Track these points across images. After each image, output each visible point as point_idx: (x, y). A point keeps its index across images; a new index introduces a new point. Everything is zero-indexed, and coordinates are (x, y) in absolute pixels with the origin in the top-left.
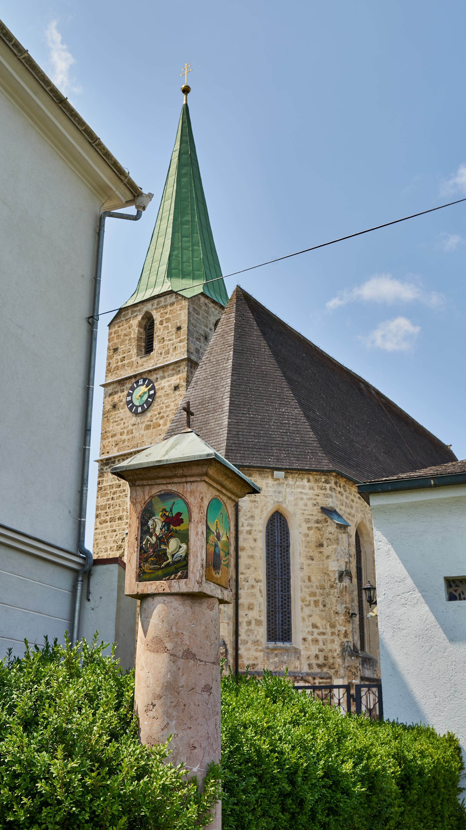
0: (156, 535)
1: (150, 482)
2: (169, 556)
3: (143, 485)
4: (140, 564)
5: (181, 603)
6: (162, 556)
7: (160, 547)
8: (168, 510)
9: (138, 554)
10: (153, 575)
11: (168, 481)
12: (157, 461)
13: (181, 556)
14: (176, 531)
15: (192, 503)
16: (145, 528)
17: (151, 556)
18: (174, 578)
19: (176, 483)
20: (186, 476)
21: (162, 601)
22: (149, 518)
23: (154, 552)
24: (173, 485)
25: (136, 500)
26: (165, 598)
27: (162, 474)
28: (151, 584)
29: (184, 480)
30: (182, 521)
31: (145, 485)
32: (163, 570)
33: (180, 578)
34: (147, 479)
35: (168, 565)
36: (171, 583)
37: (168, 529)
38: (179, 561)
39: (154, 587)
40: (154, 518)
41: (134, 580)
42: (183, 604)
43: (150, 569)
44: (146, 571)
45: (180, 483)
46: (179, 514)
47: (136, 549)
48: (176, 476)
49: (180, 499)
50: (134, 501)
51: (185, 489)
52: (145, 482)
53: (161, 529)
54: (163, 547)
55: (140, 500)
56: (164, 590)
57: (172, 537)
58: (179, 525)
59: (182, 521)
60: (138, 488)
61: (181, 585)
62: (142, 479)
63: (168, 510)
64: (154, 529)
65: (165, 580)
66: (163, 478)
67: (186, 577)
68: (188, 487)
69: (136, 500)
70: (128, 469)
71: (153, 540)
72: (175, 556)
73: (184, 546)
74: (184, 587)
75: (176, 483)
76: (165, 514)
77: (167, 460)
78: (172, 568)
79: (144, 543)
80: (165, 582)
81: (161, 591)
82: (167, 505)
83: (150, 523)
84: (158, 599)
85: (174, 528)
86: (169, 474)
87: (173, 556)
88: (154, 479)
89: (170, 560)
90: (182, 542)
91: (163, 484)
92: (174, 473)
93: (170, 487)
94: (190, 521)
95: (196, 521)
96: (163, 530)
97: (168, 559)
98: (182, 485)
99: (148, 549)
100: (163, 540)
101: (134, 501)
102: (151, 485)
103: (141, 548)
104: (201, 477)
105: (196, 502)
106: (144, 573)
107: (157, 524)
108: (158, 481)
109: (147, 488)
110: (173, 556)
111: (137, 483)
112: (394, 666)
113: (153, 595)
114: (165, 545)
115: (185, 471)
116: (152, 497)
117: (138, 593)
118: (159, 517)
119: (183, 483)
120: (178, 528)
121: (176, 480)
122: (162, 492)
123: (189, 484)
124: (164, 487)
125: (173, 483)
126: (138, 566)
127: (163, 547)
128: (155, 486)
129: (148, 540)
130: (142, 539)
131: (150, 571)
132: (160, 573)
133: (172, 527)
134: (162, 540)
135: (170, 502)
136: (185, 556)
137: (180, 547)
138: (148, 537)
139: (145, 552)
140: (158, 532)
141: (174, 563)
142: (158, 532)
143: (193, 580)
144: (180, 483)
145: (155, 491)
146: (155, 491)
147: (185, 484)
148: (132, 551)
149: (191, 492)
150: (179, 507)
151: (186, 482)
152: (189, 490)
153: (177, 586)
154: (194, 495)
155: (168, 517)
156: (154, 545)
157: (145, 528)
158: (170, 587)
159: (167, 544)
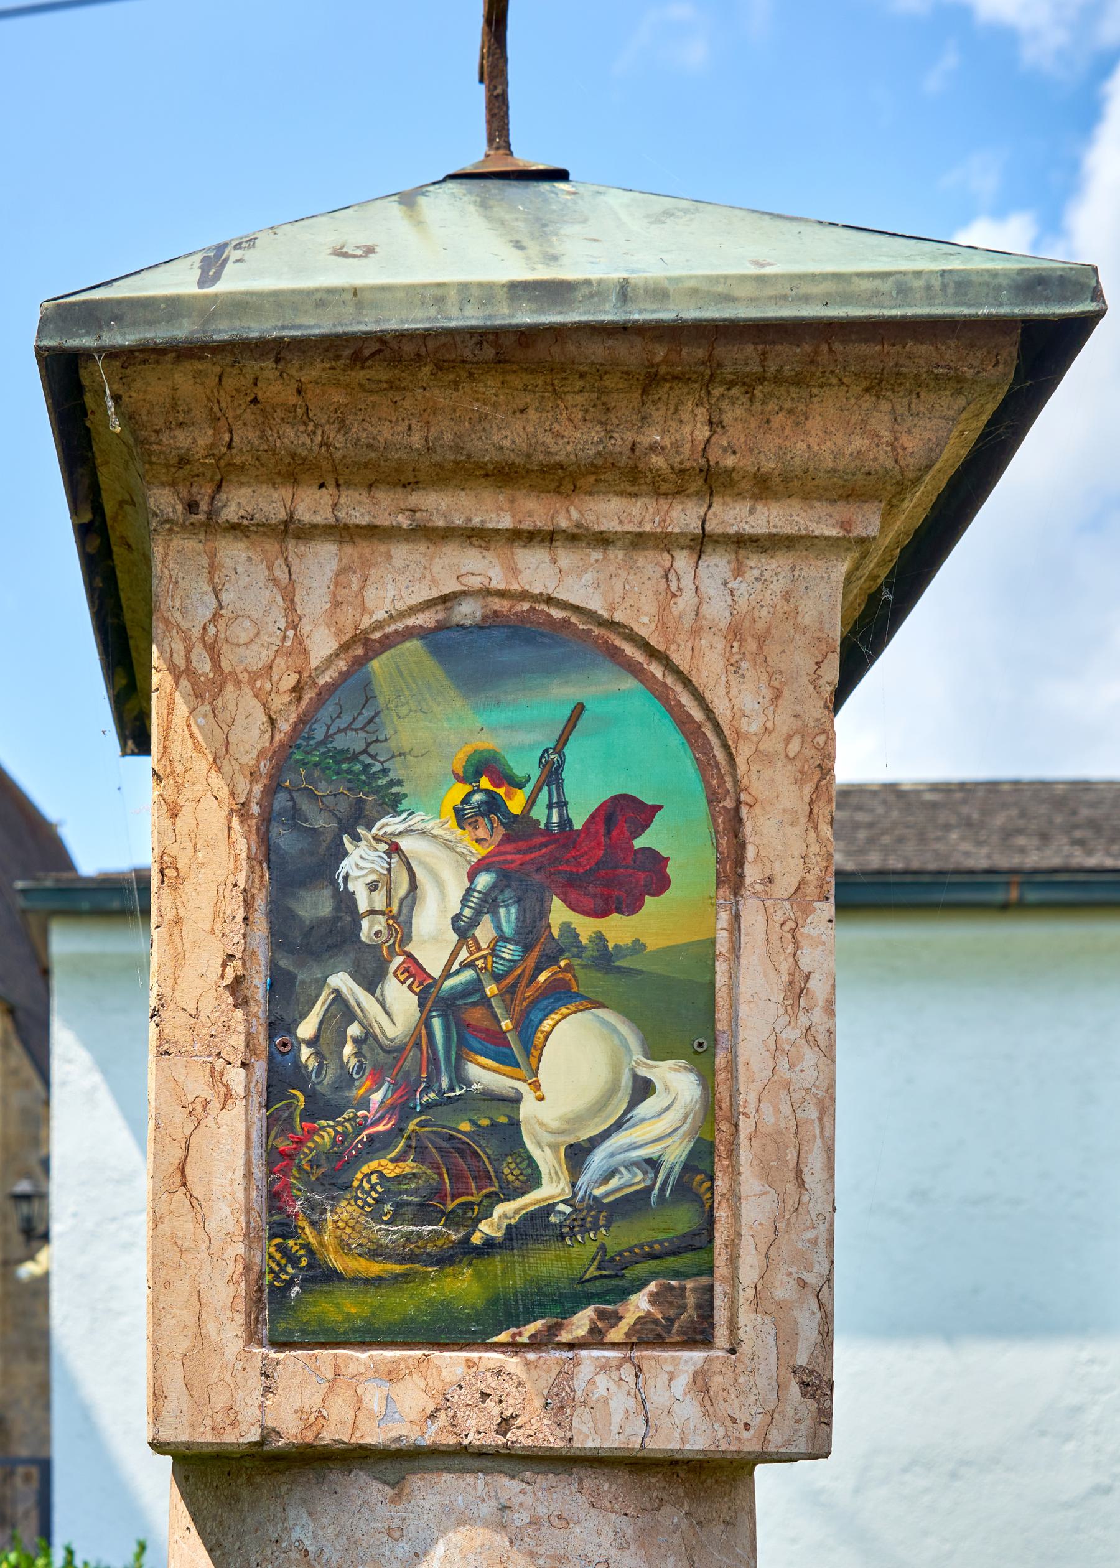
0: (413, 970)
1: (358, 509)
2: (546, 1160)
3: (291, 530)
4: (275, 1198)
5: (627, 1526)
6: (478, 1154)
7: (459, 1078)
8: (526, 766)
9: (259, 1115)
10: (404, 1304)
11: (536, 510)
12: (518, 290)
13: (653, 1164)
14: (604, 958)
15: (752, 727)
16: (316, 906)
17: (376, 1145)
18: (596, 1339)
19: (603, 540)
20: (711, 481)
21: (486, 1509)
22: (356, 819)
23: (402, 1109)
24: (567, 557)
25: (213, 651)
26: (508, 1487)
27: (510, 434)
28: (392, 1375)
29: (684, 517)
30: (654, 874)
31: (306, 533)
32: (497, 1264)
33: (650, 1336)
34: (333, 474)
35: (534, 1228)
36: (565, 1375)
37: (531, 933)
38: (632, 1205)
39: (413, 1398)
40: (390, 824)
41: (229, 1333)
42: (645, 1538)
43: (376, 1253)
44: (337, 1262)
45: (638, 541)
46: (626, 813)
47: (236, 1078)
48: (632, 476)
49: (630, 683)
50: (204, 666)
51: (685, 603)
52: (312, 505)
53: (463, 929)
54: (483, 1074)
55: (256, 657)
56: (505, 1424)
57: (561, 995)
58: (632, 906)
59: (654, 874)
60: (234, 553)
61: (658, 1398)
62: (294, 471)
63: (526, 766)
64: (400, 923)
65: (513, 1347)
66: (504, 475)
67: (700, 1335)
68: (711, 587)
69: (213, 651)
70: (223, 331)
71: (395, 1011)
72: (598, 1159)
73: (677, 1084)
74: (689, 1410)
75: (603, 540)
76: (493, 805)
77: (624, 291)
78: (580, 1255)
79: (306, 1029)
80: (513, 1363)
81: (477, 1429)
82: (515, 726)
83: (360, 863)
84: (434, 1491)
85: (586, 927)
86: (574, 437)
87: (577, 1155)
88: (404, 478)
89: (552, 1188)
90: (655, 1051)
91: (477, 536)
92: (621, 440)
93: (537, 572)
94: (731, 875)
95: (785, 885)
96: (484, 933)
97: (533, 1179)
98: (650, 563)
99: (346, 1080)
100: (496, 1015)
101: (204, 666)
102: (372, 532)
103: (281, 1079)
104: (842, 510)
105: (783, 721)
106: (321, 1276)
107: (425, 877)
108: (441, 505)
109: (320, 562)
110: (577, 1155)
111: (237, 503)
112: (85, 1414)
113: (398, 1462)
114: (506, 1059)
115: (735, 434)
116: (364, 646)
117: (269, 1433)
118: (444, 825)
119: (664, 542)
120: (618, 929)
121: (609, 512)
122: (468, 611)
123: (717, 564)
124: (482, 568)
125: (576, 537)
126: (261, 1220)
127: (483, 1074)
128: (401, 552)
129: (342, 1010)
130: (285, 998)
131: (376, 1268)
132: (462, 1286)
133: (559, 913)
134: (476, 1016)
135: (554, 699)
136: (688, 1167)
137: (643, 1089)
138: (341, 981)
139: (321, 1108)
140: (433, 943)
141: (591, 1213)
142: (433, 943)
143: (768, 1362)
144: (638, 541)
145: (401, 585)
146: (401, 585)
147: (683, 561)
148: (198, 1086)
149: (735, 633)
150: (622, 752)
151: (701, 543)
152: (717, 610)
153: (621, 1403)
154: (760, 658)
155: (518, 829)
156: (396, 1051)
157: (316, 906)
158: (559, 1405)
159: (521, 1050)
